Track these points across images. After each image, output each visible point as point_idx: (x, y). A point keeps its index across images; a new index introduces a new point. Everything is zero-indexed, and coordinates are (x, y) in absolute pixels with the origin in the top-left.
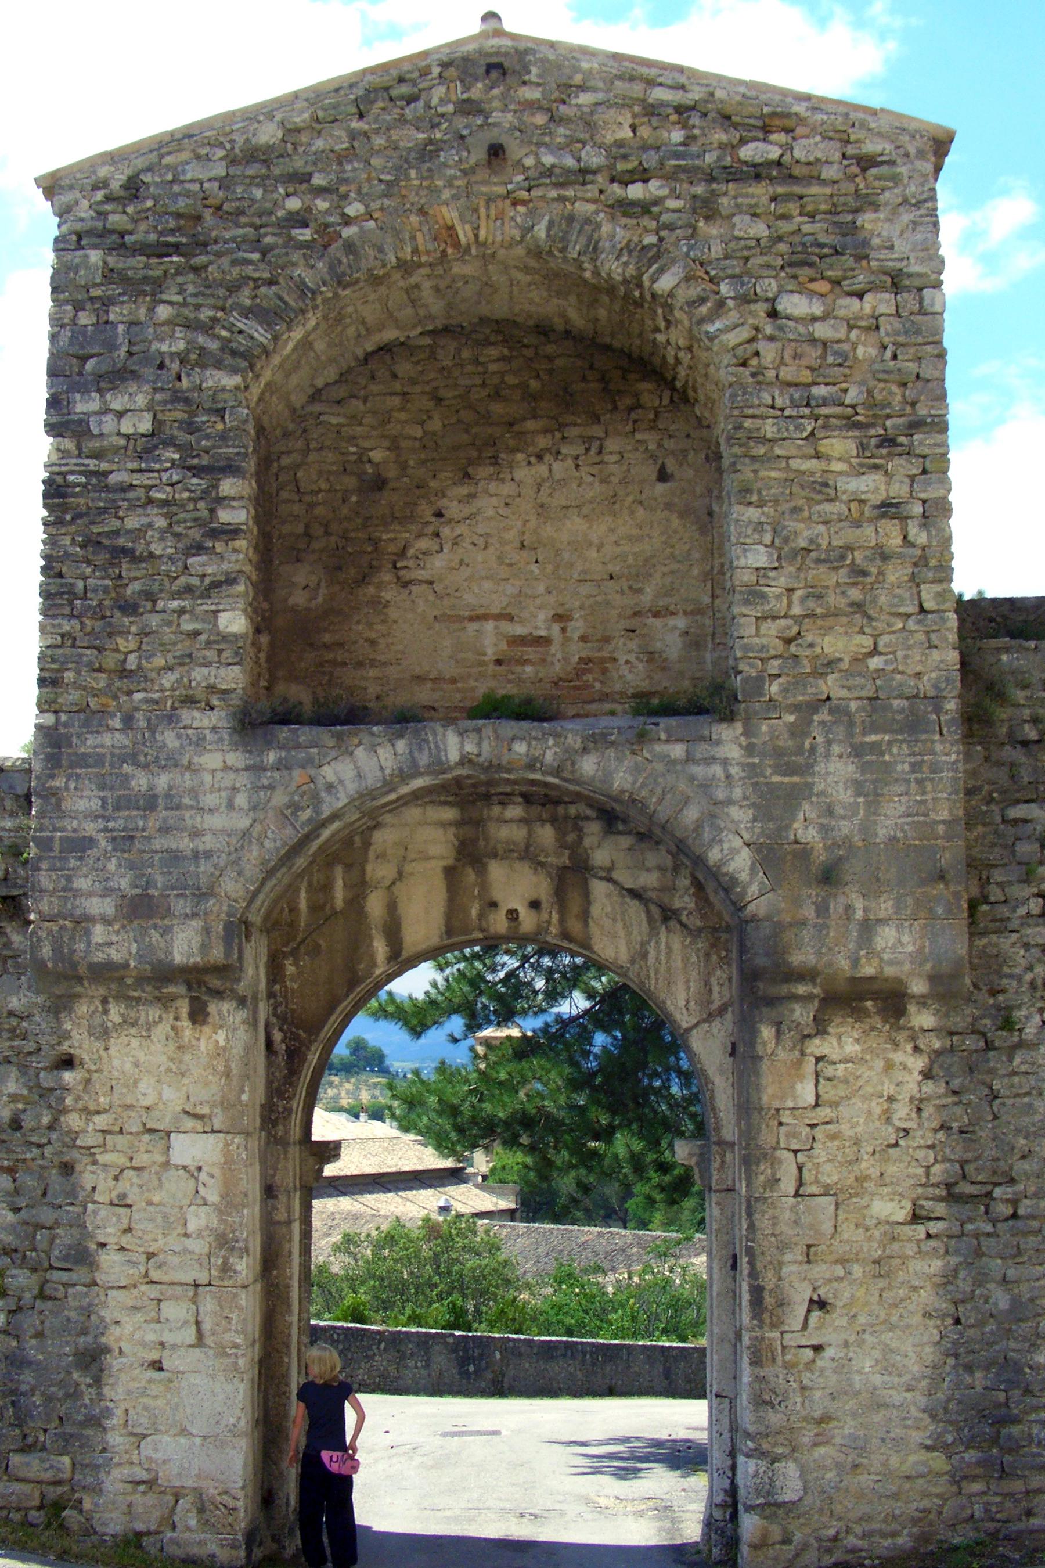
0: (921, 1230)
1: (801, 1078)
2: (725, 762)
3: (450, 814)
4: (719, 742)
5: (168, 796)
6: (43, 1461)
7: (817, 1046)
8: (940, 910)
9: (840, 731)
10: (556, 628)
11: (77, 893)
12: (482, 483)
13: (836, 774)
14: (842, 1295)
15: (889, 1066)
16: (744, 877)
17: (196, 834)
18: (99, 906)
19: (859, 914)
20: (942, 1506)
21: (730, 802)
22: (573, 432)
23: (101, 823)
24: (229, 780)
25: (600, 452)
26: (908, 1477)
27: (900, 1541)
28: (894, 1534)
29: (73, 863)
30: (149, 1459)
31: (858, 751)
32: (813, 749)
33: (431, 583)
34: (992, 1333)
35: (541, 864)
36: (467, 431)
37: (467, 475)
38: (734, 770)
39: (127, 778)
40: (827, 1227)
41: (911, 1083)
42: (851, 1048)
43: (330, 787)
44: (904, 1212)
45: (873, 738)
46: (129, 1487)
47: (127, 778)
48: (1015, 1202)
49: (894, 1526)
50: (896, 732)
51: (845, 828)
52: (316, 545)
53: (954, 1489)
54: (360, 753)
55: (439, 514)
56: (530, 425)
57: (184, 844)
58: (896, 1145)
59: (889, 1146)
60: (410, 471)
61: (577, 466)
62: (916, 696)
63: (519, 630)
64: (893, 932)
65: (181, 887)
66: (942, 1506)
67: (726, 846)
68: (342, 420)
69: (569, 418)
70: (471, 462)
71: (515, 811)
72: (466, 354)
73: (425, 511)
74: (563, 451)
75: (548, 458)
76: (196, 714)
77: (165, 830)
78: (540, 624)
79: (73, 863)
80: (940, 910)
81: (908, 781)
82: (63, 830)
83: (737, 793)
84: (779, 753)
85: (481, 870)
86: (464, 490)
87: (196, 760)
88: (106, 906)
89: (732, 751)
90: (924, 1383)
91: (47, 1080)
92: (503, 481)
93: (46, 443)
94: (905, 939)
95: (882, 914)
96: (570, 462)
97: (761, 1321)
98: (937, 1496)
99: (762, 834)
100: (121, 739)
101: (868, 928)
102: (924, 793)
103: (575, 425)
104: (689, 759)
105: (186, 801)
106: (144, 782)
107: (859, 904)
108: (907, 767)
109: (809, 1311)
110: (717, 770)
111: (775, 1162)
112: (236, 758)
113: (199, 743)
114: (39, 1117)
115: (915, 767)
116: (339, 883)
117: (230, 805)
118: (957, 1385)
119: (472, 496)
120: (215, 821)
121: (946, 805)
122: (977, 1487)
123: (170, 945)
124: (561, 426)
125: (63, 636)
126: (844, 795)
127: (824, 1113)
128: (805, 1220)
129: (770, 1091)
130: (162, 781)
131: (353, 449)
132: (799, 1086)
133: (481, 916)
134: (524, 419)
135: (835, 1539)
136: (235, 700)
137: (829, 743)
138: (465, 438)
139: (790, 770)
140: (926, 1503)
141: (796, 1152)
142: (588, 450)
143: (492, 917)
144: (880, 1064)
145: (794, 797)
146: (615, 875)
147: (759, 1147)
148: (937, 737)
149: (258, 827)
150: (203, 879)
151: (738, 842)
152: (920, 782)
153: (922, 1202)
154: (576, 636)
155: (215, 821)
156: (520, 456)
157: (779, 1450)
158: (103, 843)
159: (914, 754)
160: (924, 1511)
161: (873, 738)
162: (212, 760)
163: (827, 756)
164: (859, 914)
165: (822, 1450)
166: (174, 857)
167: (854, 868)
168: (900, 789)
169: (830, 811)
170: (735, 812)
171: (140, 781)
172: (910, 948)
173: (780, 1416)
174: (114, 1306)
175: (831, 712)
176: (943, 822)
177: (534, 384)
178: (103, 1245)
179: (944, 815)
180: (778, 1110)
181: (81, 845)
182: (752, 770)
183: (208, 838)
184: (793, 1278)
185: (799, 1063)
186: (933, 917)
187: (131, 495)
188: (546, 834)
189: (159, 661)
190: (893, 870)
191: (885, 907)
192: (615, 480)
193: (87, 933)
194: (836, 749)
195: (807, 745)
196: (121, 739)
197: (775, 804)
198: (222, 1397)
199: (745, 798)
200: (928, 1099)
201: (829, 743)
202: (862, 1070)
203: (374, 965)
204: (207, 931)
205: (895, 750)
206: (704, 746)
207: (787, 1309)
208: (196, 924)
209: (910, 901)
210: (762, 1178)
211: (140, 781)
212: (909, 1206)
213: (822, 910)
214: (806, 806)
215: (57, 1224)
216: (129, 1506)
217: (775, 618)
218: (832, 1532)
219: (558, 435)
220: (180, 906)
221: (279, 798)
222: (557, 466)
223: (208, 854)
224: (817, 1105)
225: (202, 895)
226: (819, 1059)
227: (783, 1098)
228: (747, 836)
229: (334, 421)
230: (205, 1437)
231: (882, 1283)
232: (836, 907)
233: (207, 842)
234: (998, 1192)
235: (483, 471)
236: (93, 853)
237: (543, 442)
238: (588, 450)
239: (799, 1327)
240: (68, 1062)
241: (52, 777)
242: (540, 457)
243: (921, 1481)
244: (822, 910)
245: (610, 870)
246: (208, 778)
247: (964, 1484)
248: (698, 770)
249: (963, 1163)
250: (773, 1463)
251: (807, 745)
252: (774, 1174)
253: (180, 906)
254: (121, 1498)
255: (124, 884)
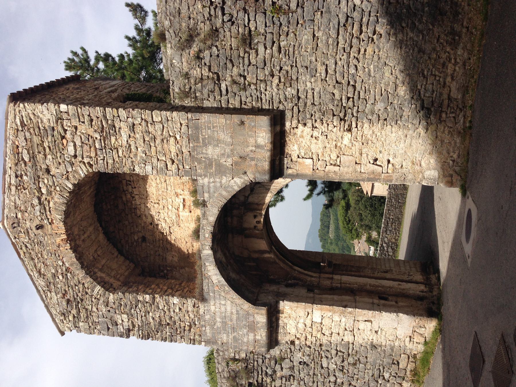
0: (354, 130)
1: (304, 162)
2: (209, 182)
3: (230, 236)
4: (203, 184)
5: (222, 319)
6: (402, 361)
7: (294, 158)
8: (253, 124)
9: (199, 149)
10: (180, 197)
11: (248, 341)
12: (142, 212)
13: (212, 152)
14: (372, 155)
15: (302, 137)
16: (242, 180)
17: (232, 313)
18: (251, 336)
19: (254, 148)
20: (448, 127)
21: (221, 182)
22: (125, 188)
23: (230, 334)
24: (218, 305)
25: (130, 181)
26: (436, 137)
27: (458, 141)
28: (455, 143)
29: (240, 341)
30: (404, 337)
31: (205, 145)
32: (205, 158)
33: (170, 227)
34: (391, 109)
35: (244, 214)
36: (127, 215)
37: (140, 216)
38: (212, 180)
39: (218, 327)
40: (351, 158)
41: (307, 130)
42: (296, 147)
43: (219, 282)
44: (348, 134)
45: (201, 140)
46: (411, 342)
47: (218, 327)
48: (349, 98)
49: (453, 142)
50: (199, 133)
51: (228, 150)
52: (161, 254)
53: (443, 123)
54: (209, 274)
55: (151, 224)
56: (124, 199)
57: (235, 317)
58: (327, 135)
59: (327, 138)
60: (140, 230)
61: (135, 188)
62: (188, 126)
63: (181, 206)
64: (259, 139)
65: (246, 318)
66: (448, 127)
67: (233, 184)
68: (127, 245)
69: (121, 189)
70: (136, 215)
71: (229, 219)
72: (106, 213)
73: (151, 227)
74: (131, 191)
75: (133, 195)
76: (201, 310)
77: (231, 320)
78: (179, 201)
79: (240, 341)
80: (253, 124)
81: (213, 131)
82: (231, 343)
83: (218, 180)
84: (205, 167)
85: (246, 229)
86: (144, 217)
87: (213, 312)
88: (251, 336)
89: (206, 180)
90: (405, 131)
91: (298, 348)
92: (140, 207)
93: (133, 339)
94: (261, 135)
95: (254, 141)
96: (134, 190)
97: (378, 179)
98: (444, 128)
99: (230, 175)
100: (208, 328)
101: (258, 146)
102: (217, 126)
103: (123, 187)
104: (209, 192)
105: (223, 315)
106: (219, 324)
107: (251, 148)
108: (209, 131)
109: (377, 165)
110: (212, 185)
111: (329, 172)
112: (212, 303)
113: (209, 311)
114: (307, 350)
115: (209, 128)
116: (249, 264)
117: (225, 305)
118: (407, 121)
119: (145, 216)
120: (229, 308)
121: (220, 120)
122: (444, 115)
123: (261, 322)
124: (124, 191)
125: (181, 338)
126: (218, 150)
127: (315, 157)
128: (347, 164)
129: (307, 172)
130: (218, 320)
131: (135, 243)
132: (306, 164)
133: (258, 230)
134: (122, 200)
135: (453, 161)
136: (196, 301)
137: (202, 153)
138: (129, 216)
139: (211, 165)
140: (446, 132)
141: (326, 165)
142: (130, 185)
143: (259, 228)
144: (301, 139)
145: (219, 165)
146: (247, 195)
147: (324, 176)
148: (200, 121)
149: (230, 299)
150: (244, 313)
151: (232, 181)
152: (214, 127)
153: (345, 129)
154: (182, 192)
155: (229, 308)
156: (133, 202)
157: (420, 176)
158: (235, 334)
159: (205, 128)
160: (449, 133)
161: (201, 140)
162: (213, 308)
163: (207, 154)
164: (254, 148)
165: (423, 163)
166: (238, 319)
167: (239, 150)
168: (216, 133)
169: (223, 155)
170: (224, 181)
171: (219, 325)
172: (264, 134)
173: (409, 175)
174: (359, 340)
175: (193, 152)
176: (226, 121)
177: (113, 197)
178: (342, 339)
179: (223, 121)
180: (313, 170)
181: (235, 339)
182: (211, 175)
183: (233, 311)
184: (366, 168)
185: (299, 163)
186: (255, 126)
187: (144, 320)
188: (235, 212)
189: (187, 318)
190: (240, 137)
191: (252, 141)
192: (138, 178)
193: (258, 340)
194: (204, 151)
195: (204, 159)
196: (208, 328)
197: (221, 170)
198: (387, 318)
199: (220, 178)
200: (313, 125)
201: (202, 153)
202: (303, 145)
203: (271, 257)
204: (257, 313)
205: (204, 134)
206: (205, 187)
207: (375, 171)
208: (256, 316)
209: (250, 133)
210: (334, 176)
211: (219, 325)
212: (346, 133)
213: (253, 159)
214: (221, 161)
215: (337, 350)
216: (417, 343)
217: (167, 165)
218: (451, 162)
219: (126, 192)
220: (251, 319)
221: (223, 294)
222: (135, 193)
223: (237, 311)
224: (312, 159)
225: (248, 314)
226: (299, 157)
227: (310, 168)
228: (230, 179)
229: (127, 247)
230: (398, 323)
231: (370, 142)
232: (252, 155)
233: (234, 311)
234: (344, 105)
235: (138, 212)
236: (237, 336)
237: (129, 196)
238: (130, 185)
239: (381, 168)
240: (293, 343)
241: (218, 344)
242: (133, 197)
243: (438, 134)
244: (253, 159)
245: (245, 196)
246: (217, 309)
247: (442, 119)
248: (212, 190)
249: (334, 115)
250: (424, 178)
251: (204, 159)
252: (333, 172)
253: (251, 319)
254: (414, 345)
255: (245, 331)
